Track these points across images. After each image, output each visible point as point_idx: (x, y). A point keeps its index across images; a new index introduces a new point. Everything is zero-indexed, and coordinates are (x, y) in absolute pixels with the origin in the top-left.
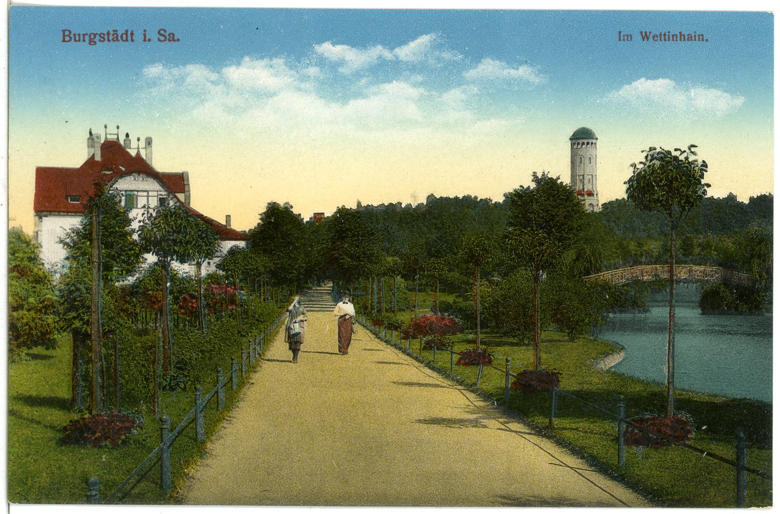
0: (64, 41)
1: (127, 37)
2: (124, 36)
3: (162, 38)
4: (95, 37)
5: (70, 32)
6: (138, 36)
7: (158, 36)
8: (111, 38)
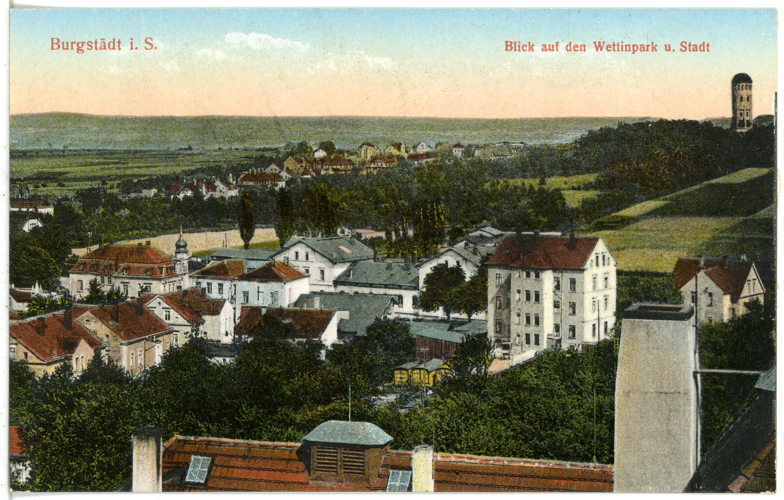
0: (52, 48)
1: (704, 48)
2: (112, 44)
4: (83, 46)
5: (59, 40)
6: (660, 48)
8: (98, 46)
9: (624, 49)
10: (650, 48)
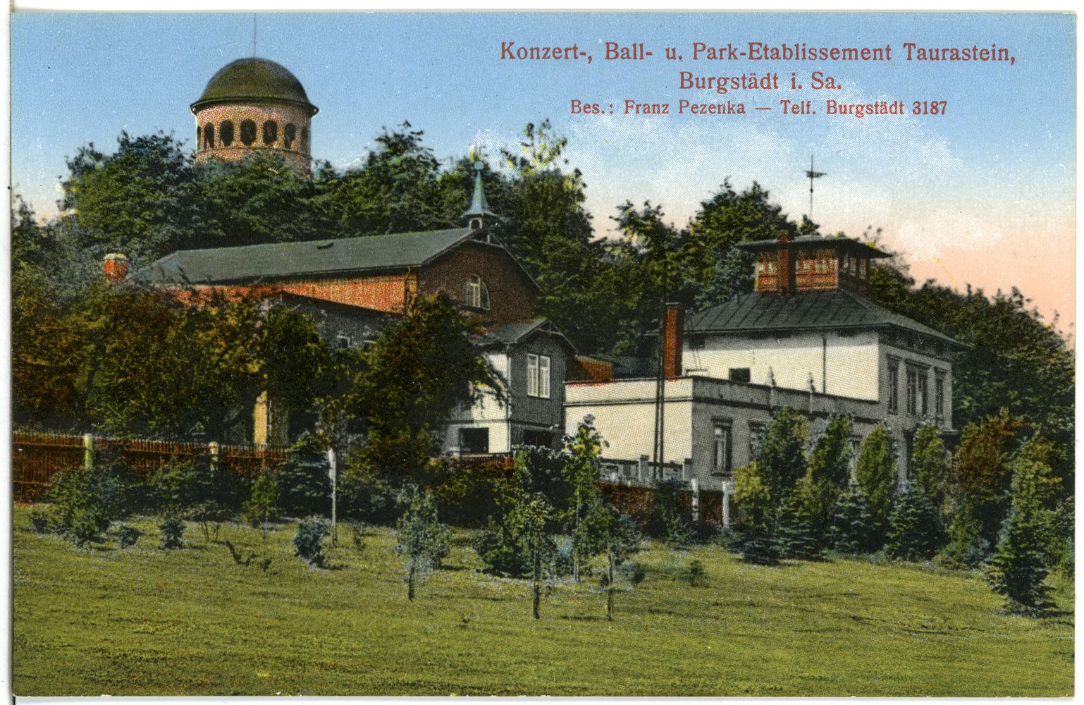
0: (608, 57)
3: (818, 84)
4: (725, 83)
5: (691, 75)
7: (811, 80)
8: (747, 84)
9: (997, 57)
10: (725, 54)
